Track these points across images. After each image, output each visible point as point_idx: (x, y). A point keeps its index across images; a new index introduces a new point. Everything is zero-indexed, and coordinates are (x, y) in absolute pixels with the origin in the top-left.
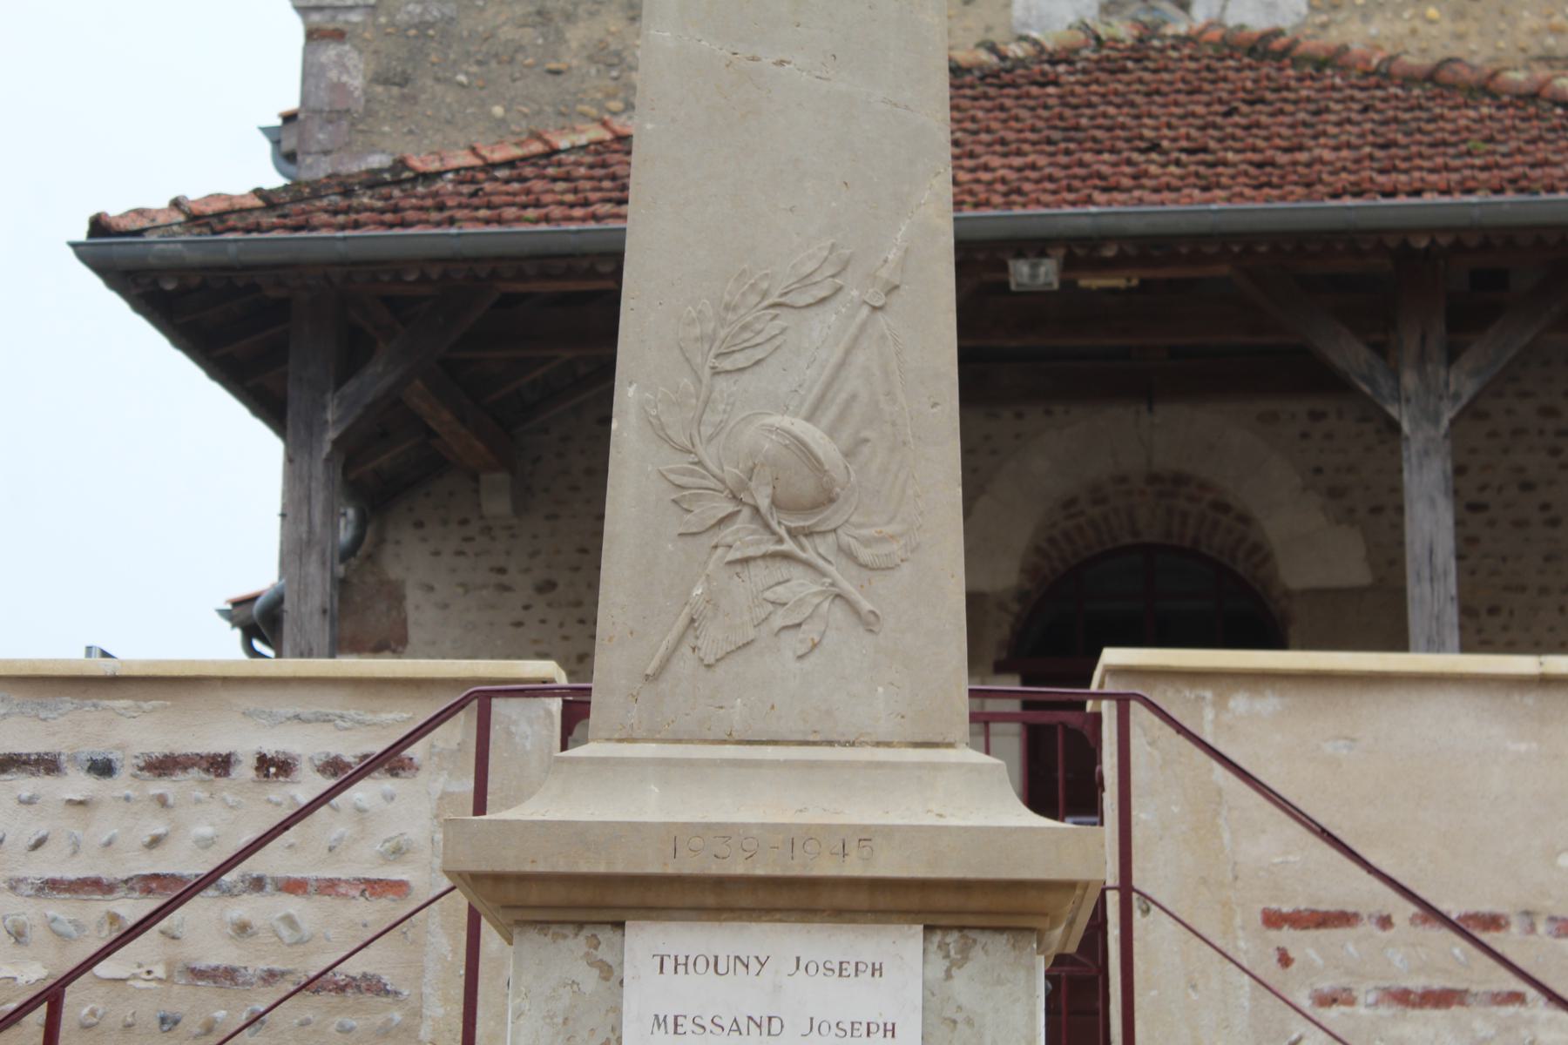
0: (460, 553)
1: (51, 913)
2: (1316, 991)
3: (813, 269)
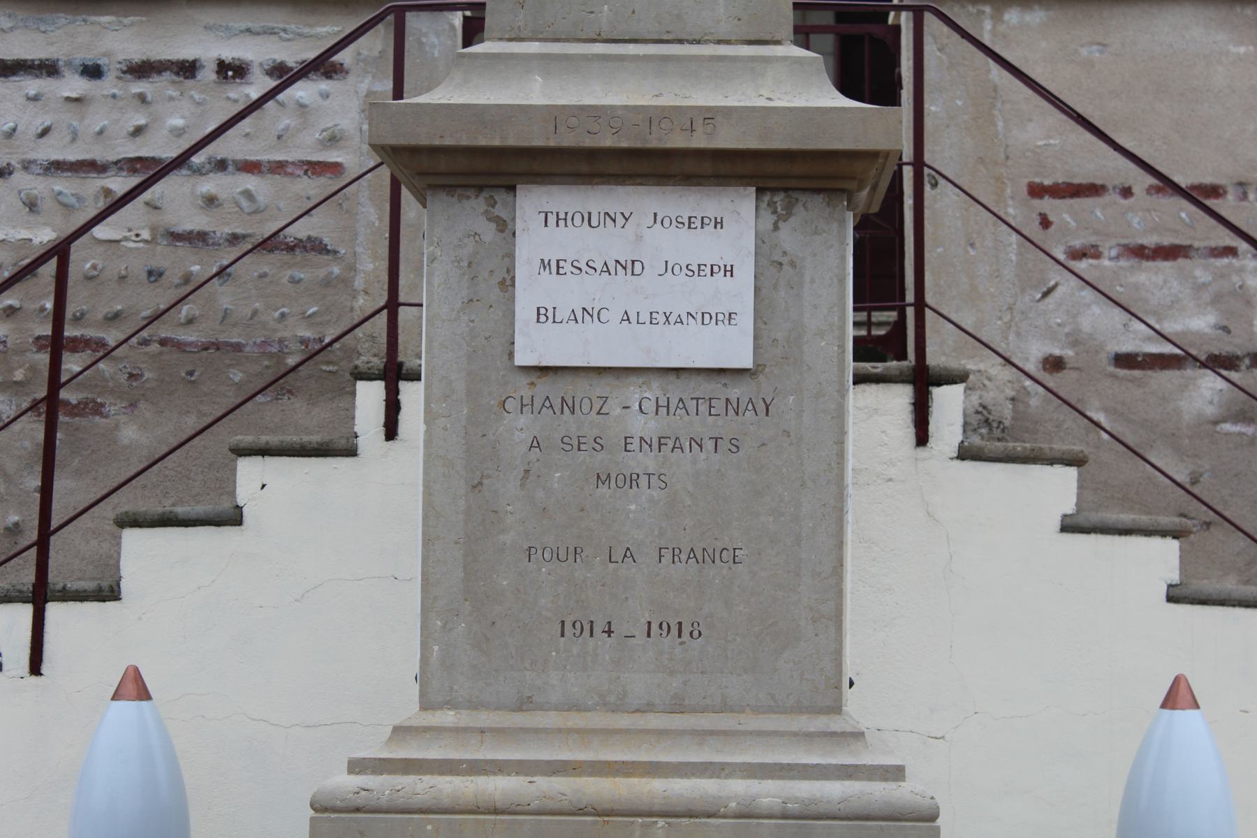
1: (57, 188)
2: (1070, 247)
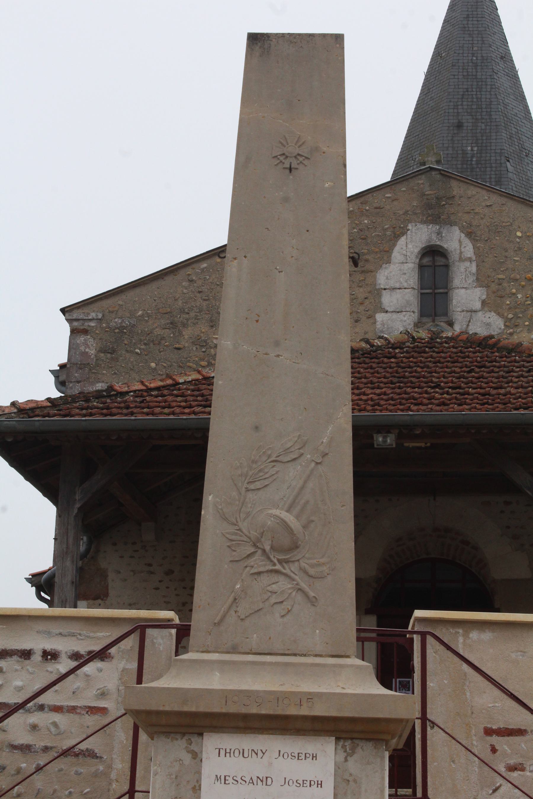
0: (132, 557)
3: (290, 446)
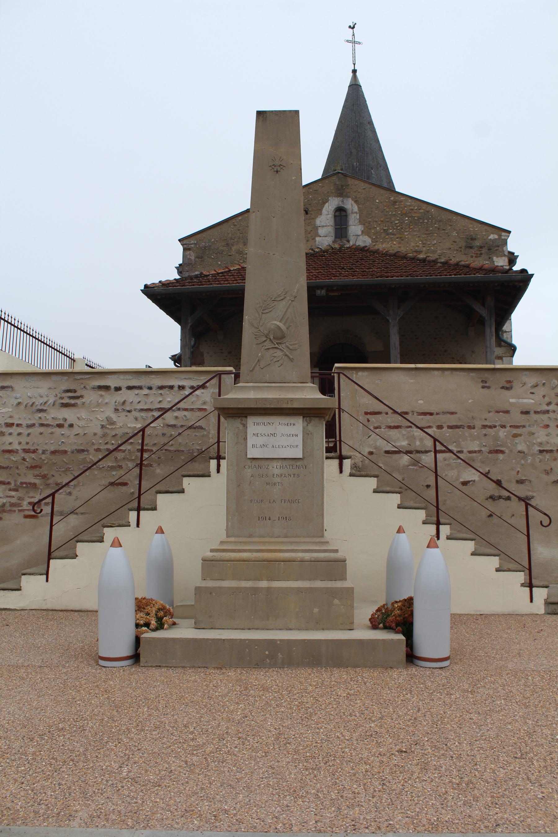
0: (213, 346)
1: (142, 415)
